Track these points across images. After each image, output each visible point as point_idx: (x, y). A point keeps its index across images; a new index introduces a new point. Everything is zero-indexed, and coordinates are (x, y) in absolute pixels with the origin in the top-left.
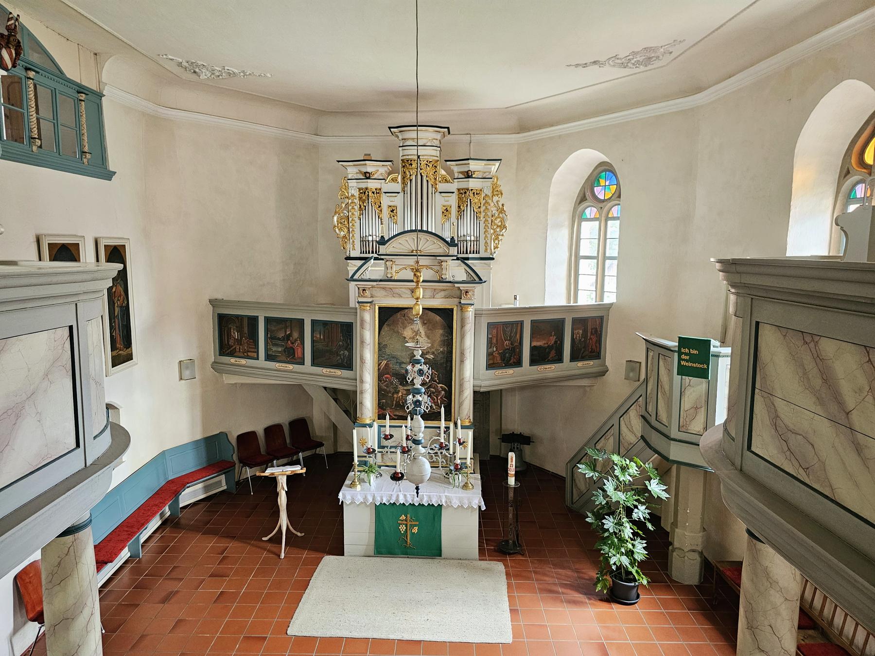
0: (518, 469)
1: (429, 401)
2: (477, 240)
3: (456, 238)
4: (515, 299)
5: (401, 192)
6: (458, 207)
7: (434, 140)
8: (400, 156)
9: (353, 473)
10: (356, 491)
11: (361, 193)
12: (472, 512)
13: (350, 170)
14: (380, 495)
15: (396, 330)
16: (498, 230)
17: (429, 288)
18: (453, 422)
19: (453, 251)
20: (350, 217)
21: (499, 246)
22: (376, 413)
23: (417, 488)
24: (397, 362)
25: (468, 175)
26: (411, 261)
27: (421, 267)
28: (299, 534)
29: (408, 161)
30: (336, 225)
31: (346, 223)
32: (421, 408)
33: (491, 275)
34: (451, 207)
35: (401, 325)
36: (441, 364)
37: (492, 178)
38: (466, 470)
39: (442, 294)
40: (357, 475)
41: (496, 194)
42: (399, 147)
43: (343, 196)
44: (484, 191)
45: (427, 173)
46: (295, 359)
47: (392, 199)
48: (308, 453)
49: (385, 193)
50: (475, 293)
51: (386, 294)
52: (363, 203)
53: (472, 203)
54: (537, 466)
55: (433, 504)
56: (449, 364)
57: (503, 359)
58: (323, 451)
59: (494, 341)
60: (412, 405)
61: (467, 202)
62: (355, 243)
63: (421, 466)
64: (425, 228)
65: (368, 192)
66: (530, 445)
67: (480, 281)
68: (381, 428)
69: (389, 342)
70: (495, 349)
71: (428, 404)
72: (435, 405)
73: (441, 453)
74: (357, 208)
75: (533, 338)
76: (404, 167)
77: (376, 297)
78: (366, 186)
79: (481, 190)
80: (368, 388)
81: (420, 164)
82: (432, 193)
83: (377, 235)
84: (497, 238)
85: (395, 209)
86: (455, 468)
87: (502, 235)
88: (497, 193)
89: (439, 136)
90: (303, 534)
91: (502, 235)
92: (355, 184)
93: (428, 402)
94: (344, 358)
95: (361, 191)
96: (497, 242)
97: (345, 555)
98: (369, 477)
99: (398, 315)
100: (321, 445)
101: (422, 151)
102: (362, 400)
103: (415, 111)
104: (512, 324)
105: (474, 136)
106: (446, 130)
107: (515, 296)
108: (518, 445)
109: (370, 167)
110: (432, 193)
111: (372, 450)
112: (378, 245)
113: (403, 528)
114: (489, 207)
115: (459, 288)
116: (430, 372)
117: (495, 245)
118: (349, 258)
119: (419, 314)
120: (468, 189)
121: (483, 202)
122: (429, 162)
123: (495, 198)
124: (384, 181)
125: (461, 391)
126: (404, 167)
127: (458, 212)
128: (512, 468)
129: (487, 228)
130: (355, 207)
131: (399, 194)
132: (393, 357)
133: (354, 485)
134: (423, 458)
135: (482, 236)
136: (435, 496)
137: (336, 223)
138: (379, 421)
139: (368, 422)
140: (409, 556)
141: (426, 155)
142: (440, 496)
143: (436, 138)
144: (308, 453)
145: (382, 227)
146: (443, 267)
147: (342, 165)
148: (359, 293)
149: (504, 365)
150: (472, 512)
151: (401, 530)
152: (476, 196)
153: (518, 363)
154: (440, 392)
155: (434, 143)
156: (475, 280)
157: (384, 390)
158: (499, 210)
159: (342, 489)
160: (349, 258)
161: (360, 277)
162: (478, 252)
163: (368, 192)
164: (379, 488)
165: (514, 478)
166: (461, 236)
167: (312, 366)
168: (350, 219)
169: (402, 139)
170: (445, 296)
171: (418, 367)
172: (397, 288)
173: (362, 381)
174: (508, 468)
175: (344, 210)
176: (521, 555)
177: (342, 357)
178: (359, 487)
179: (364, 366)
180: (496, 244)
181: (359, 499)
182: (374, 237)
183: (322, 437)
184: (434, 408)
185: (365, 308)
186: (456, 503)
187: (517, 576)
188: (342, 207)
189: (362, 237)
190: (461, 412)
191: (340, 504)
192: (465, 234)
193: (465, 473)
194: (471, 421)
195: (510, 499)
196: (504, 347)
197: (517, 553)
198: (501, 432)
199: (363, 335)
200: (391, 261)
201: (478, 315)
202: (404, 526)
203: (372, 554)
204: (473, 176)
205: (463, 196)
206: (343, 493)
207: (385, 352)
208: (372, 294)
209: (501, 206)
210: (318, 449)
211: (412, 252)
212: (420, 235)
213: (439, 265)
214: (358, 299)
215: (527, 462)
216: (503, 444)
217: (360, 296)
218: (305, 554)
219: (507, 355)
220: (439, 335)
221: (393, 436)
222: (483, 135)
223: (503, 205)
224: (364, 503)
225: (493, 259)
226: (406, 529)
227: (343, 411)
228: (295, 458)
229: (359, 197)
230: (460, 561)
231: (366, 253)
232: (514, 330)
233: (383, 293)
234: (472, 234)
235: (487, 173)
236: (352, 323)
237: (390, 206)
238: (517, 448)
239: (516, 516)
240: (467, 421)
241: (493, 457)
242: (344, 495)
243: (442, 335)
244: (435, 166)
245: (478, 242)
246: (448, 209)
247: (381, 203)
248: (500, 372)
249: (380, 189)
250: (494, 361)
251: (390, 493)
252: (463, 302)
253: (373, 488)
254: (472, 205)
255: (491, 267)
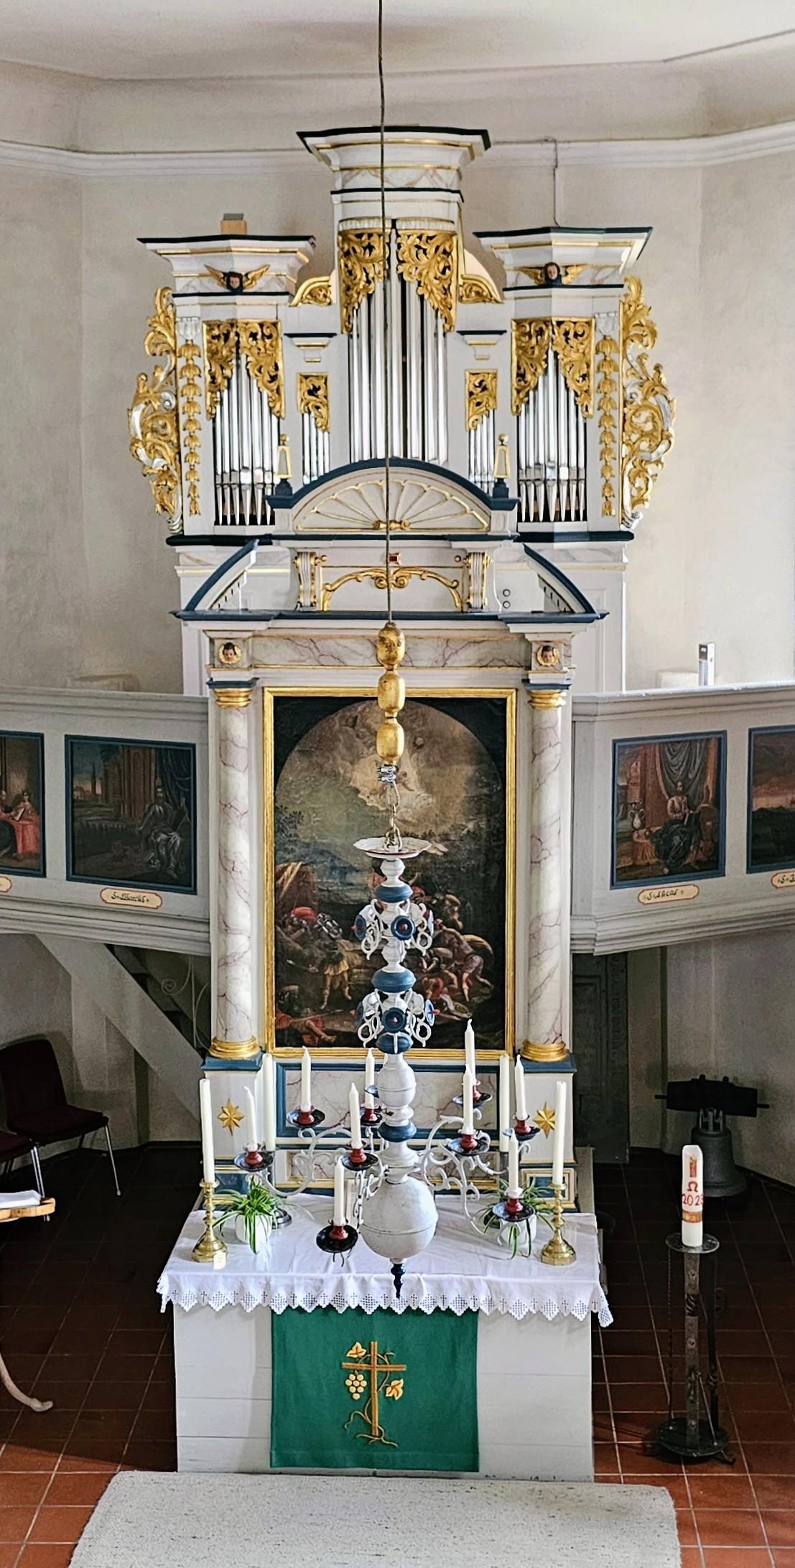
0: (716, 1194)
1: (428, 1010)
2: (579, 478)
3: (511, 485)
4: (703, 655)
5: (338, 332)
6: (518, 375)
7: (440, 171)
8: (336, 222)
9: (202, 1213)
10: (211, 1269)
11: (214, 337)
12: (570, 1331)
13: (179, 265)
14: (287, 1282)
15: (327, 767)
16: (644, 445)
17: (430, 637)
18: (511, 1051)
19: (505, 522)
20: (180, 411)
21: (647, 495)
22: (269, 1027)
23: (397, 1271)
24: (333, 868)
25: (547, 278)
26: (373, 553)
27: (406, 572)
28: (36, 1405)
29: (360, 236)
30: (140, 437)
31: (169, 429)
32: (405, 1031)
33: (624, 584)
34: (495, 376)
35: (344, 751)
36: (471, 871)
37: (621, 286)
38: (550, 1202)
39: (472, 653)
40: (214, 1222)
41: (636, 335)
42: (333, 193)
43: (159, 348)
44: (600, 326)
45: (420, 274)
46: (16, 858)
47: (311, 354)
48: (56, 1148)
49: (291, 336)
50: (573, 652)
51: (296, 657)
52: (222, 368)
53: (561, 363)
54: (778, 1182)
55: (449, 1309)
56: (494, 871)
57: (662, 853)
58: (104, 1140)
59: (635, 796)
60: (379, 1022)
61: (546, 361)
62: (198, 491)
63: (407, 1204)
64: (415, 453)
65: (237, 334)
66: (754, 1115)
67: (588, 613)
68: (287, 1072)
69: (310, 805)
70: (637, 822)
71: (426, 1021)
72: (453, 999)
73: (467, 1165)
74: (203, 382)
75: (756, 785)
76: (347, 254)
77: (266, 665)
78: (231, 317)
79: (589, 323)
80: (243, 949)
81: (399, 246)
82: (436, 335)
83: (267, 467)
84: (640, 472)
85: (323, 386)
86: (506, 1211)
87: (658, 462)
88: (638, 331)
89: (454, 158)
90: (49, 1405)
91: (658, 462)
92: (197, 311)
93: (427, 1014)
94: (168, 853)
95: (216, 332)
96: (640, 482)
97: (179, 1469)
98: (250, 1224)
99: (336, 721)
100: (100, 1121)
101: (398, 206)
102: (226, 986)
103: (378, 218)
104: (689, 741)
105: (566, 145)
106: (478, 138)
107: (701, 646)
108: (717, 1116)
109: (242, 257)
110: (436, 335)
111: (260, 1159)
112: (268, 508)
113: (357, 1384)
114: (614, 376)
115: (522, 636)
116: (430, 924)
117: (635, 493)
118: (179, 539)
119: (394, 755)
120: (547, 322)
121: (595, 360)
122: (424, 238)
123: (634, 349)
124: (286, 298)
125: (534, 957)
126: (347, 254)
127: (518, 392)
128: (693, 1194)
129: (608, 440)
130: (198, 381)
131: (334, 338)
132: (322, 853)
133: (205, 1251)
134: (413, 1180)
135: (595, 466)
136: (456, 1285)
137: (139, 431)
138: (279, 1049)
139: (245, 1053)
140: (378, 1471)
141: (415, 219)
142: (471, 1283)
143: (446, 164)
144: (56, 1148)
145: (283, 453)
146: (471, 571)
147: (155, 251)
148: (213, 654)
149: (666, 871)
150: (570, 1331)
151: (353, 1390)
152: (573, 342)
153: (712, 864)
154: (467, 959)
155: (441, 178)
156: (572, 612)
157: (296, 955)
158: (647, 385)
159: (168, 1265)
160: (179, 539)
161: (216, 607)
162: (581, 516)
163: (237, 334)
164: (283, 1259)
165: (701, 1223)
166: (528, 467)
167: (68, 879)
168: (183, 419)
169: (342, 169)
170: (479, 660)
171: (394, 911)
172: (331, 638)
173: (225, 928)
174: (680, 1195)
175: (162, 388)
176: (725, 1467)
177: (163, 852)
178: (220, 1259)
179: (231, 880)
180: (640, 489)
181: (222, 1296)
182: (258, 473)
183: (98, 1096)
184: (452, 1008)
185: (233, 702)
186: (521, 1305)
187: (713, 1530)
188: (156, 380)
189: (219, 472)
190: (533, 1019)
191: (163, 1310)
192: (542, 461)
193: (546, 1210)
194: (567, 1047)
195: (689, 1290)
196: (667, 816)
197: (709, 1457)
198: (664, 1076)
199: (227, 783)
200: (312, 554)
201: (581, 717)
202: (361, 1377)
203: (266, 1465)
204: (565, 281)
205: (534, 341)
206: (170, 1277)
207: (296, 835)
208: (253, 658)
209: (651, 372)
210: (89, 1136)
211: (376, 527)
212: (398, 474)
213: (460, 564)
214: (209, 673)
215: (749, 1171)
216: (672, 1114)
217: (217, 663)
218: (57, 1468)
219: (677, 839)
220: (463, 782)
221: (323, 1116)
222: (595, 144)
223: (657, 368)
224: (235, 1308)
225: (628, 536)
226: (369, 1387)
227: (166, 1013)
228: (17, 1163)
229: (209, 350)
230: (538, 1486)
231: (233, 523)
232: (698, 761)
233: (288, 652)
234: (564, 460)
235: (609, 271)
236: (194, 746)
237: (306, 377)
238: (716, 1127)
239: (709, 1341)
240: (555, 1047)
241: (638, 1154)
242: (174, 1283)
243: (469, 781)
244: (445, 252)
245: (582, 485)
246: (488, 382)
247: (276, 368)
248: (656, 893)
249: (275, 324)
250: (635, 859)
251: (319, 1275)
252: (534, 678)
253: (265, 1260)
254: (561, 371)
255: (625, 560)
